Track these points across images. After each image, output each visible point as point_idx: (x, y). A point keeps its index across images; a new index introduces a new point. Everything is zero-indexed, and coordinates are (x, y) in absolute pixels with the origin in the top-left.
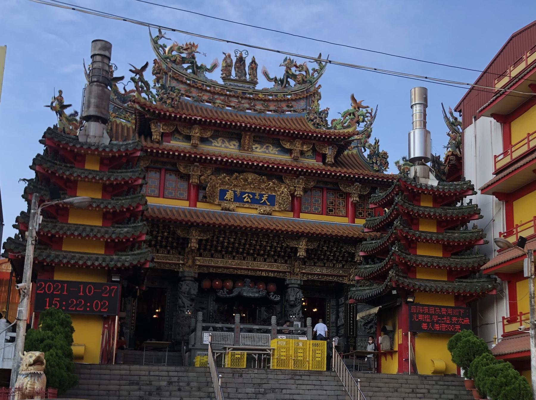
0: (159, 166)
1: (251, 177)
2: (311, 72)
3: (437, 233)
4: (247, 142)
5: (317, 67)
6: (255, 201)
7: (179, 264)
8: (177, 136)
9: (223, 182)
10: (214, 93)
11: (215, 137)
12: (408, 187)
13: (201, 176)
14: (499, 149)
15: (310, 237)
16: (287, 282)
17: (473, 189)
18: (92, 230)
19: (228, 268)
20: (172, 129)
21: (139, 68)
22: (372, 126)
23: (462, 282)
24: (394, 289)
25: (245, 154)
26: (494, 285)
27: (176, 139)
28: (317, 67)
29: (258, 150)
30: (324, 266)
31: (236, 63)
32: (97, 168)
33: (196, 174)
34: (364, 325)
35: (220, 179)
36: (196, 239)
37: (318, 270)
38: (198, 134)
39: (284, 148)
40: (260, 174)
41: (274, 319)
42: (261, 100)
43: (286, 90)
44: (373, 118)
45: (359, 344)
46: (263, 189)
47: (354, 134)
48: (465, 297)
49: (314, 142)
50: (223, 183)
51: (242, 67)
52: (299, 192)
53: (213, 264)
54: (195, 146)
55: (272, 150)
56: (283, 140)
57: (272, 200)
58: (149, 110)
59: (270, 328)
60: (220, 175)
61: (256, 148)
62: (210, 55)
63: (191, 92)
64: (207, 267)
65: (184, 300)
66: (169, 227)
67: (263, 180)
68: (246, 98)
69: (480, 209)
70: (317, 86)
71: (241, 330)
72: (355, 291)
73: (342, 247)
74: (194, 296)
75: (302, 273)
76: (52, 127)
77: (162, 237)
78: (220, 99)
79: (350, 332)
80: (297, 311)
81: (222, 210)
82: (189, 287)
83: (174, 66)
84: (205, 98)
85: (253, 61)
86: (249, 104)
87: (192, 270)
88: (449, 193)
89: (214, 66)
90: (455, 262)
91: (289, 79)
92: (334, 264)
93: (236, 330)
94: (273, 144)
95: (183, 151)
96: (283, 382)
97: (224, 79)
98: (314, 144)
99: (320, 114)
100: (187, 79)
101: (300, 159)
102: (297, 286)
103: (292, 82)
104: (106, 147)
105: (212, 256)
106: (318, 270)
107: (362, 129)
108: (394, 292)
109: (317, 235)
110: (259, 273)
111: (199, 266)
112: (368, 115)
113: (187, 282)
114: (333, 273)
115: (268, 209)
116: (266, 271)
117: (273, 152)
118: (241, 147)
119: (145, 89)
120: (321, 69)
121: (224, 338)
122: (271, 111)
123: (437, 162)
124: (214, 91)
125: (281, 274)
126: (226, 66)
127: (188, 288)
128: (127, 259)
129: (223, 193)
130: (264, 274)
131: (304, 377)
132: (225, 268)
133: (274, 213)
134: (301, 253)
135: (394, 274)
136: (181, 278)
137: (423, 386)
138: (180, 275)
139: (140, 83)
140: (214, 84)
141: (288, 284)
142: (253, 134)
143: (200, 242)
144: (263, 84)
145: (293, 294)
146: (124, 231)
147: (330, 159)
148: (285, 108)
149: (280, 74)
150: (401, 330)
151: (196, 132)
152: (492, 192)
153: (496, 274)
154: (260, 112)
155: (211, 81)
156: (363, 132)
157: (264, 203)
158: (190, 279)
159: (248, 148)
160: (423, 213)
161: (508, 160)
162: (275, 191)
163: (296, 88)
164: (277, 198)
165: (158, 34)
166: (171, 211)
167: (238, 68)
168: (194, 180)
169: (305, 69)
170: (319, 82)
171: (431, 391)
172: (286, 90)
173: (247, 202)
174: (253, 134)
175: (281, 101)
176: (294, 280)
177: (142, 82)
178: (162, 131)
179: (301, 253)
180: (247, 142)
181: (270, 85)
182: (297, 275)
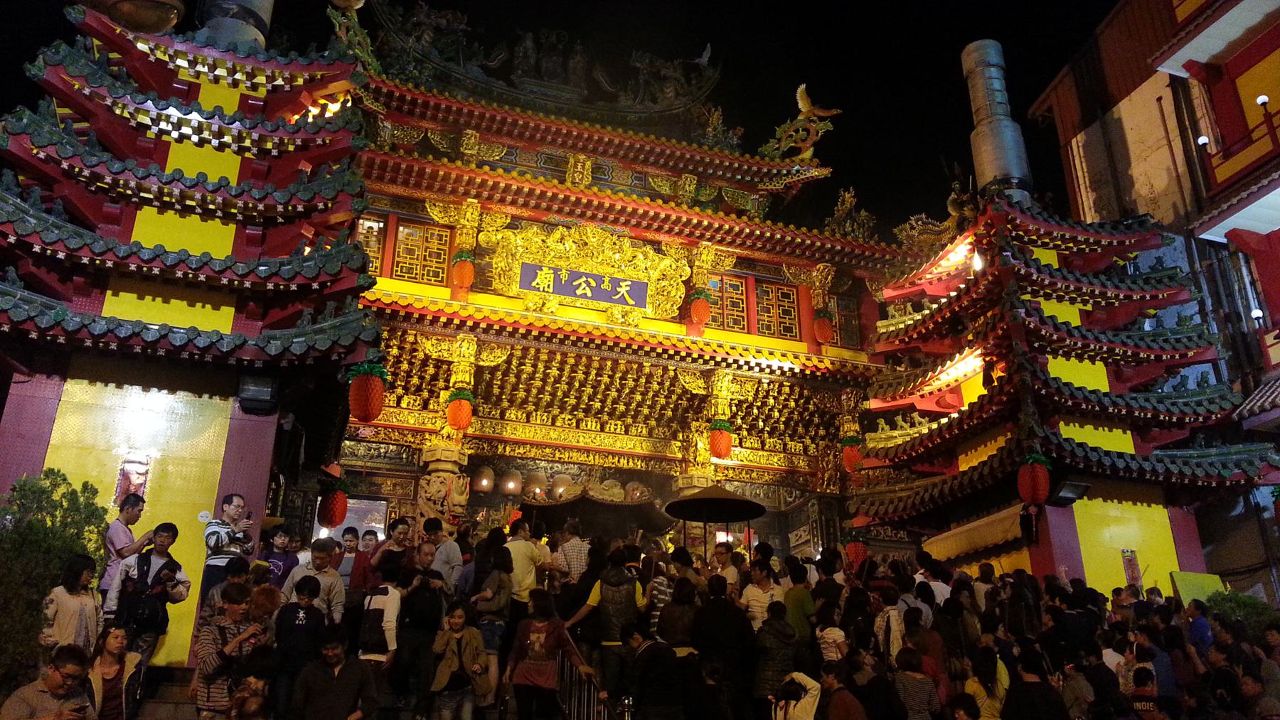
18: (926, 491)
74: (460, 510)
98: (720, 189)
158: (449, 466)
173: (584, 296)
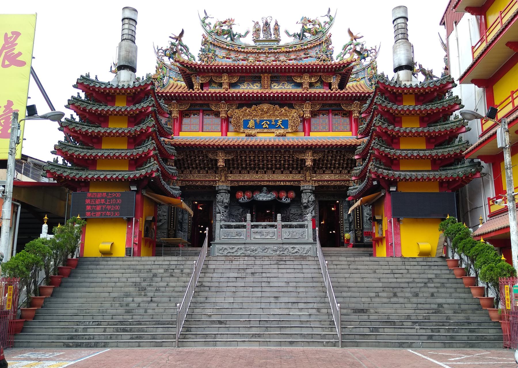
1: (265, 107)
2: (323, 24)
4: (266, 82)
5: (328, 20)
6: (272, 126)
7: (216, 181)
8: (213, 85)
10: (247, 53)
12: (387, 88)
13: (228, 111)
14: (477, 38)
15: (314, 149)
16: (301, 189)
17: (453, 82)
19: (253, 181)
20: (207, 79)
22: (376, 60)
23: (446, 170)
24: (374, 180)
26: (477, 169)
27: (213, 88)
28: (328, 20)
29: (276, 87)
30: (332, 173)
31: (263, 27)
33: (223, 109)
34: (369, 219)
37: (326, 177)
38: (227, 81)
41: (279, 216)
43: (303, 42)
47: (352, 61)
48: (448, 182)
49: (320, 74)
55: (287, 86)
56: (294, 76)
57: (285, 124)
59: (276, 223)
61: (274, 86)
62: (244, 27)
64: (237, 181)
65: (220, 207)
66: (202, 152)
67: (276, 109)
69: (460, 100)
70: (328, 34)
72: (352, 190)
73: (344, 156)
75: (313, 180)
79: (357, 226)
80: (310, 211)
81: (246, 136)
82: (224, 198)
83: (217, 37)
84: (241, 57)
85: (276, 24)
86: (274, 57)
87: (225, 185)
88: (429, 89)
89: (247, 33)
90: (440, 152)
91: (305, 33)
92: (341, 171)
93: (247, 227)
96: (267, 267)
97: (255, 41)
100: (227, 45)
103: (307, 34)
105: (240, 173)
106: (326, 177)
108: (375, 183)
110: (278, 183)
112: (372, 51)
114: (340, 178)
115: (281, 131)
116: (283, 181)
117: (288, 87)
118: (262, 87)
119: (185, 51)
120: (331, 20)
123: (430, 76)
124: (246, 52)
125: (296, 183)
126: (255, 31)
127: (222, 198)
129: (246, 122)
130: (282, 184)
131: (288, 263)
132: (251, 181)
133: (287, 135)
134: (309, 163)
135: (373, 167)
136: (218, 191)
137: (403, 267)
142: (270, 75)
144: (285, 40)
145: (305, 197)
147: (335, 86)
148: (303, 56)
149: (298, 30)
150: (386, 218)
151: (225, 79)
152: (470, 79)
153: (478, 157)
156: (368, 66)
157: (279, 127)
161: (484, 45)
162: (287, 116)
163: (311, 39)
164: (290, 122)
165: (204, 16)
167: (265, 31)
168: (223, 115)
169: (317, 23)
170: (331, 31)
171: (410, 271)
172: (303, 42)
173: (266, 128)
176: (307, 186)
177: (181, 46)
178: (200, 82)
179: (309, 163)
180: (266, 82)
181: (291, 40)
182: (309, 182)
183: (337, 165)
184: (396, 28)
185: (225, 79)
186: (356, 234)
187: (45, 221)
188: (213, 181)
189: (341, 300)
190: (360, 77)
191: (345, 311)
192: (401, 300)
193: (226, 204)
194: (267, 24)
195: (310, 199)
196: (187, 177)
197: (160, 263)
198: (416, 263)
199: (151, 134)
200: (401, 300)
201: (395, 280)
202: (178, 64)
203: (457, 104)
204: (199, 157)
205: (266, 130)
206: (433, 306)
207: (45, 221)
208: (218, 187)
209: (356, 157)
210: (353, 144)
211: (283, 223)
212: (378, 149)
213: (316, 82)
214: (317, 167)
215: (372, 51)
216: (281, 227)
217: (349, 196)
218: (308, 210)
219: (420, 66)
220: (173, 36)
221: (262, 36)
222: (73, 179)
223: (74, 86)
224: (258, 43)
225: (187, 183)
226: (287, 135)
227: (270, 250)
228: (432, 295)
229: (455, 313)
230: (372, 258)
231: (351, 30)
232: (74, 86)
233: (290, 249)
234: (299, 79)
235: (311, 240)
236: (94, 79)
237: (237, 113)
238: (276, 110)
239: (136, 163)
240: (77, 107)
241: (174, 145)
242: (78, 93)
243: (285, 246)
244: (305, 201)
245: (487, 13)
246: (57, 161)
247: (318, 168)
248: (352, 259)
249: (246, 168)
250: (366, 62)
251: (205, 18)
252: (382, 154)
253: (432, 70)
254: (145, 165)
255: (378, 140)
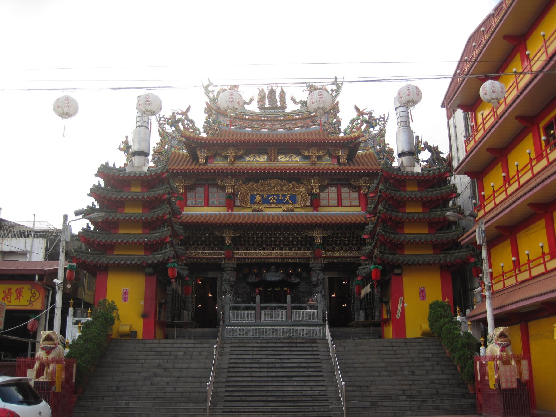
0: (203, 182)
1: (273, 182)
2: (330, 92)
3: (423, 213)
5: (334, 87)
6: (279, 201)
8: (218, 157)
9: (252, 189)
11: (247, 154)
13: (234, 186)
15: (324, 226)
16: (311, 266)
21: (184, 110)
22: (386, 128)
23: (446, 253)
25: (272, 165)
29: (283, 160)
32: (139, 190)
35: (249, 187)
36: (230, 237)
39: (304, 155)
40: (282, 179)
41: (289, 298)
42: (290, 120)
44: (385, 122)
45: (376, 314)
46: (285, 191)
47: (359, 137)
50: (252, 190)
51: (273, 97)
52: (316, 190)
53: (248, 256)
54: (314, 163)
57: (293, 199)
58: (193, 140)
59: (285, 305)
60: (249, 183)
61: (281, 158)
63: (234, 123)
64: (243, 258)
68: (277, 120)
70: (335, 102)
71: (262, 308)
76: (105, 164)
77: (249, 238)
78: (257, 124)
81: (253, 211)
82: (229, 276)
86: (280, 124)
87: (230, 262)
89: (252, 100)
94: (295, 154)
95: (217, 169)
97: (260, 108)
98: (328, 149)
99: (334, 124)
101: (317, 162)
102: (318, 268)
104: (146, 173)
105: (247, 249)
107: (377, 132)
109: (329, 224)
110: (286, 260)
111: (237, 258)
112: (381, 120)
113: (228, 272)
115: (290, 206)
117: (296, 160)
121: (248, 316)
122: (266, 129)
125: (305, 260)
126: (261, 99)
128: (159, 257)
129: (253, 198)
130: (290, 261)
132: (258, 258)
133: (295, 210)
135: (378, 253)
137: (405, 348)
138: (223, 266)
139: (186, 122)
140: (252, 113)
141: (312, 268)
142: (277, 148)
143: (323, 238)
144: (291, 107)
146: (156, 235)
147: (343, 160)
148: (310, 124)
151: (231, 152)
154: (289, 130)
155: (250, 111)
156: (377, 135)
159: (274, 159)
160: (415, 197)
162: (295, 192)
166: (301, 216)
173: (273, 203)
174: (277, 148)
175: (306, 118)
179: (318, 241)
181: (297, 107)
183: (347, 242)
184: (398, 116)
185: (231, 152)
186: (366, 313)
187: (71, 305)
188: (219, 258)
189: (347, 379)
190: (369, 146)
191: (350, 389)
192: (399, 378)
193: (232, 283)
194: (272, 92)
195: (320, 277)
196: (192, 254)
197: (179, 345)
198: (417, 344)
199: (166, 221)
200: (399, 378)
201: (396, 360)
202: (183, 139)
203: (454, 193)
204: (205, 234)
205: (273, 205)
206: (426, 382)
207: (71, 305)
208: (224, 264)
209: (364, 237)
210: (362, 222)
211: (293, 305)
212: (383, 236)
213: (324, 155)
214: (327, 243)
215: (381, 120)
216: (290, 308)
217: (358, 276)
218: (317, 289)
219: (426, 143)
220: (180, 112)
221: (267, 104)
222: (95, 265)
223: (96, 175)
224: (263, 111)
225: (192, 260)
226: (295, 210)
227: (279, 332)
228: (427, 373)
229: (443, 387)
230: (381, 340)
231: (358, 106)
232: (96, 175)
233: (300, 331)
234: (307, 152)
235: (321, 321)
236: (112, 166)
237: (244, 189)
238: (285, 185)
239: (152, 247)
240: (98, 195)
241: (181, 224)
242: (99, 182)
243: (295, 328)
244: (314, 279)
245: (476, 111)
246: (81, 248)
247: (327, 245)
248: (359, 341)
249: (253, 245)
250: (375, 130)
251: (208, 86)
252: (387, 240)
253: (437, 147)
254: (161, 250)
255: (383, 226)
